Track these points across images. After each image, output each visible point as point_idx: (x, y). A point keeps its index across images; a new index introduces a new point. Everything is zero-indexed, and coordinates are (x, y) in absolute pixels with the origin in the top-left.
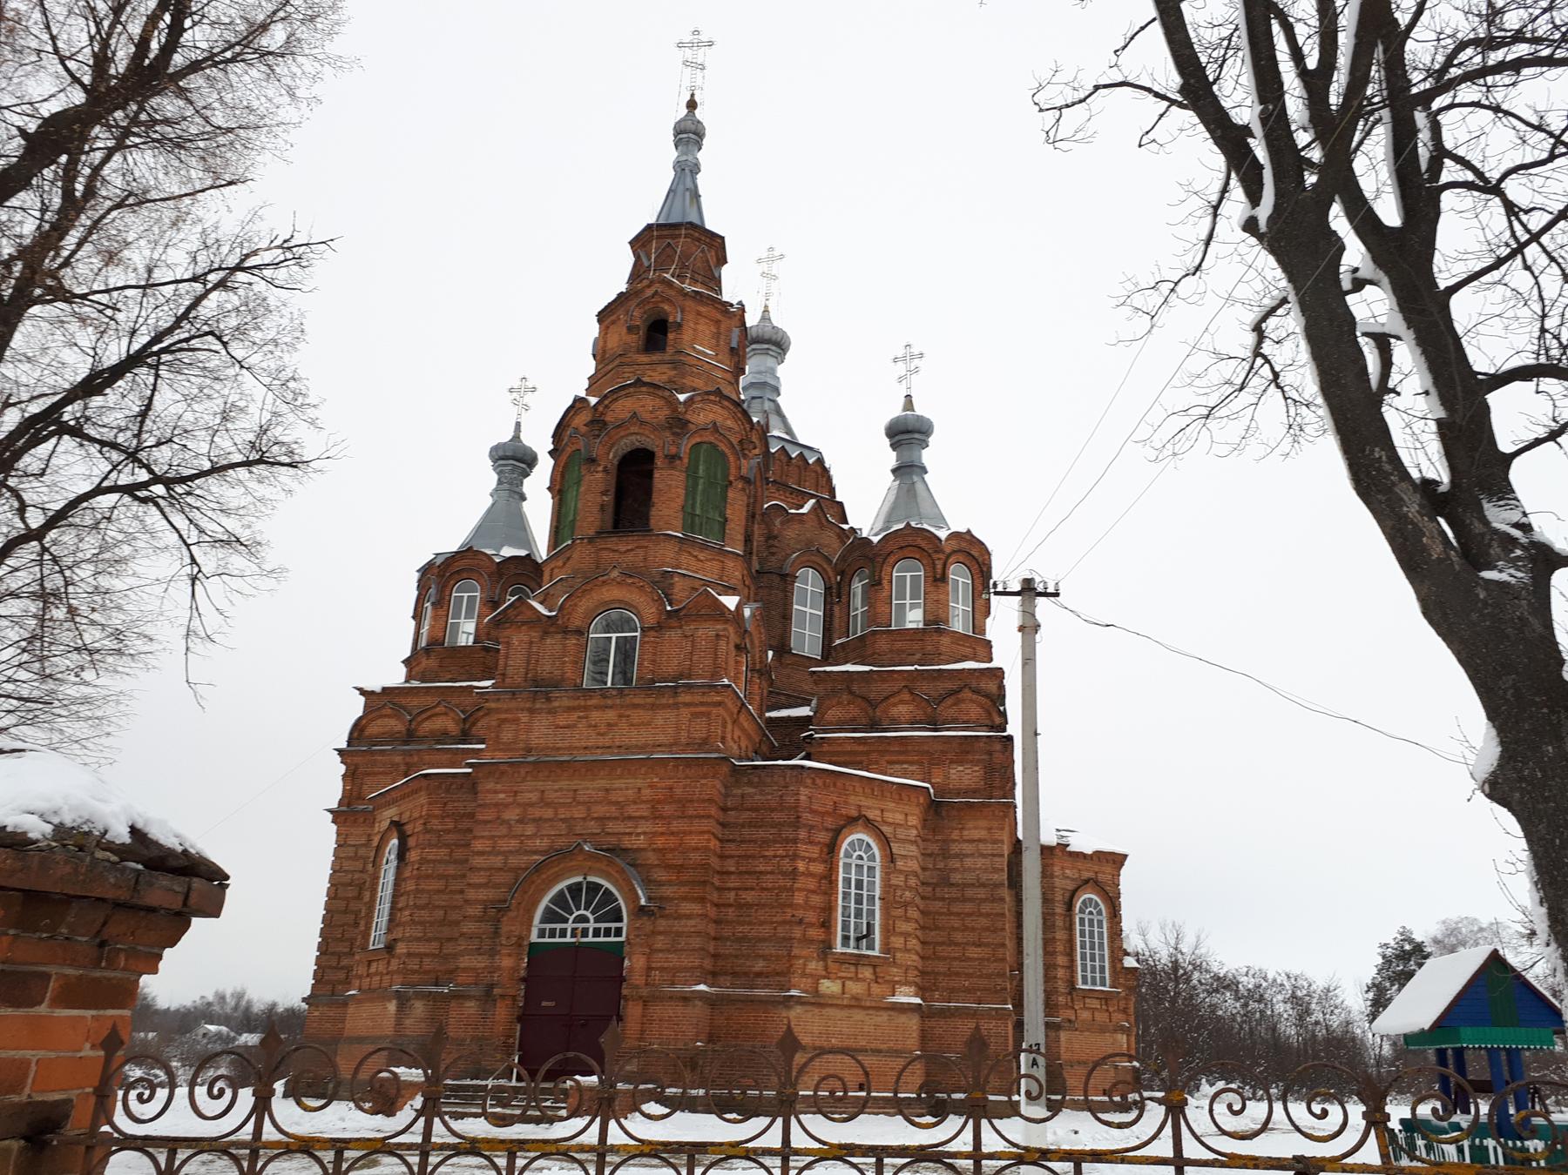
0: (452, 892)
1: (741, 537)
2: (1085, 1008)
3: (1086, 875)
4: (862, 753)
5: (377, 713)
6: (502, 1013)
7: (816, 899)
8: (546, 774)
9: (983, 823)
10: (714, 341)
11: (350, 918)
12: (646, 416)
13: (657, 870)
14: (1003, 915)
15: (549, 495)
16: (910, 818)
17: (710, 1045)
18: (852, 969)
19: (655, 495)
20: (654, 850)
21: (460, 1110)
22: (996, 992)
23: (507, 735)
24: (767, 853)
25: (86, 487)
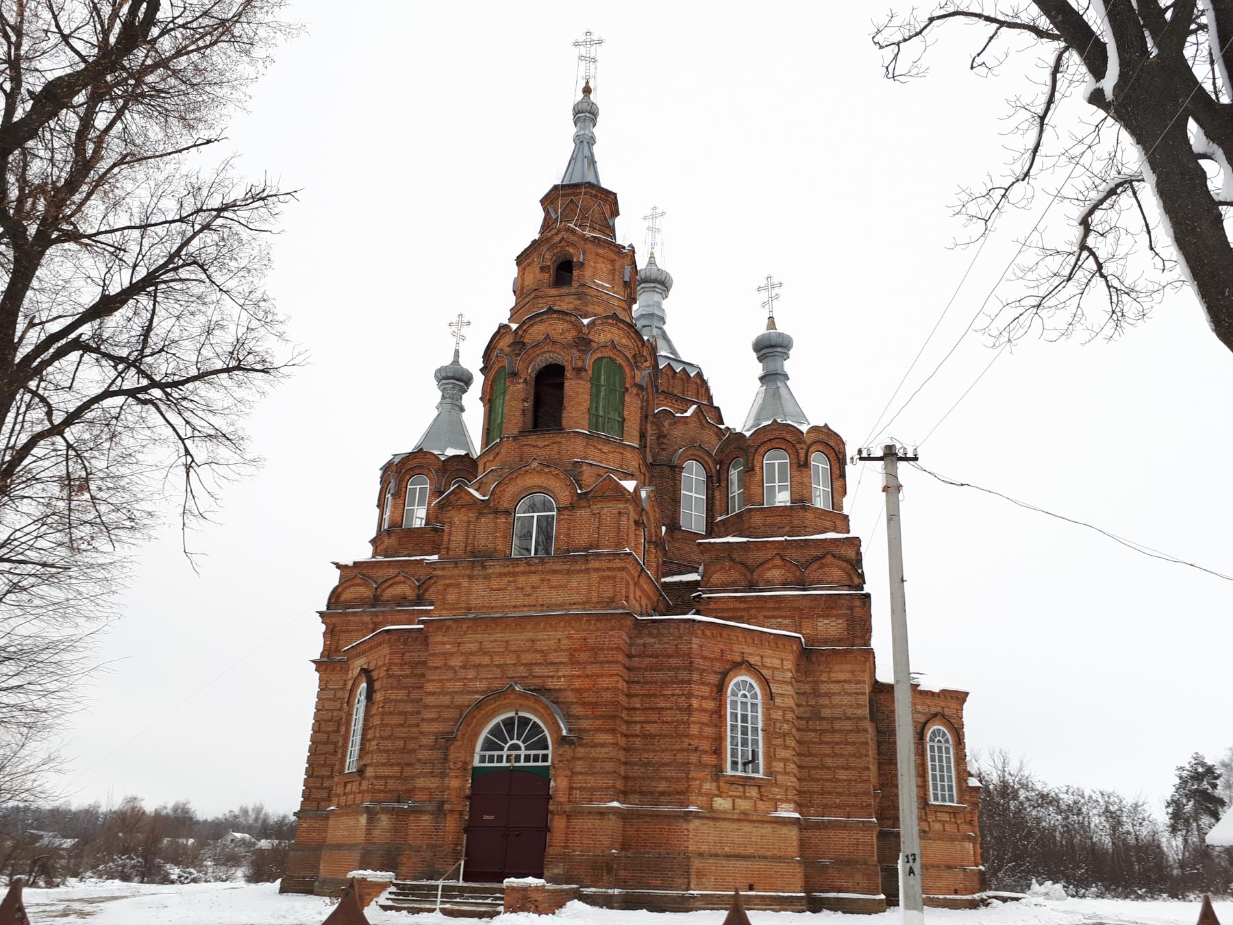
0: (410, 726)
1: (636, 433)
2: (937, 820)
3: (934, 710)
4: (744, 609)
5: (350, 583)
6: (451, 825)
7: (709, 731)
8: (483, 628)
9: (848, 667)
10: (610, 277)
11: (331, 748)
12: (557, 337)
13: (575, 706)
14: (867, 743)
15: (481, 404)
16: (785, 663)
17: (624, 853)
18: (741, 789)
19: (565, 401)
20: (572, 690)
21: (416, 906)
22: (863, 808)
23: (451, 598)
24: (666, 693)
25: (97, 390)
